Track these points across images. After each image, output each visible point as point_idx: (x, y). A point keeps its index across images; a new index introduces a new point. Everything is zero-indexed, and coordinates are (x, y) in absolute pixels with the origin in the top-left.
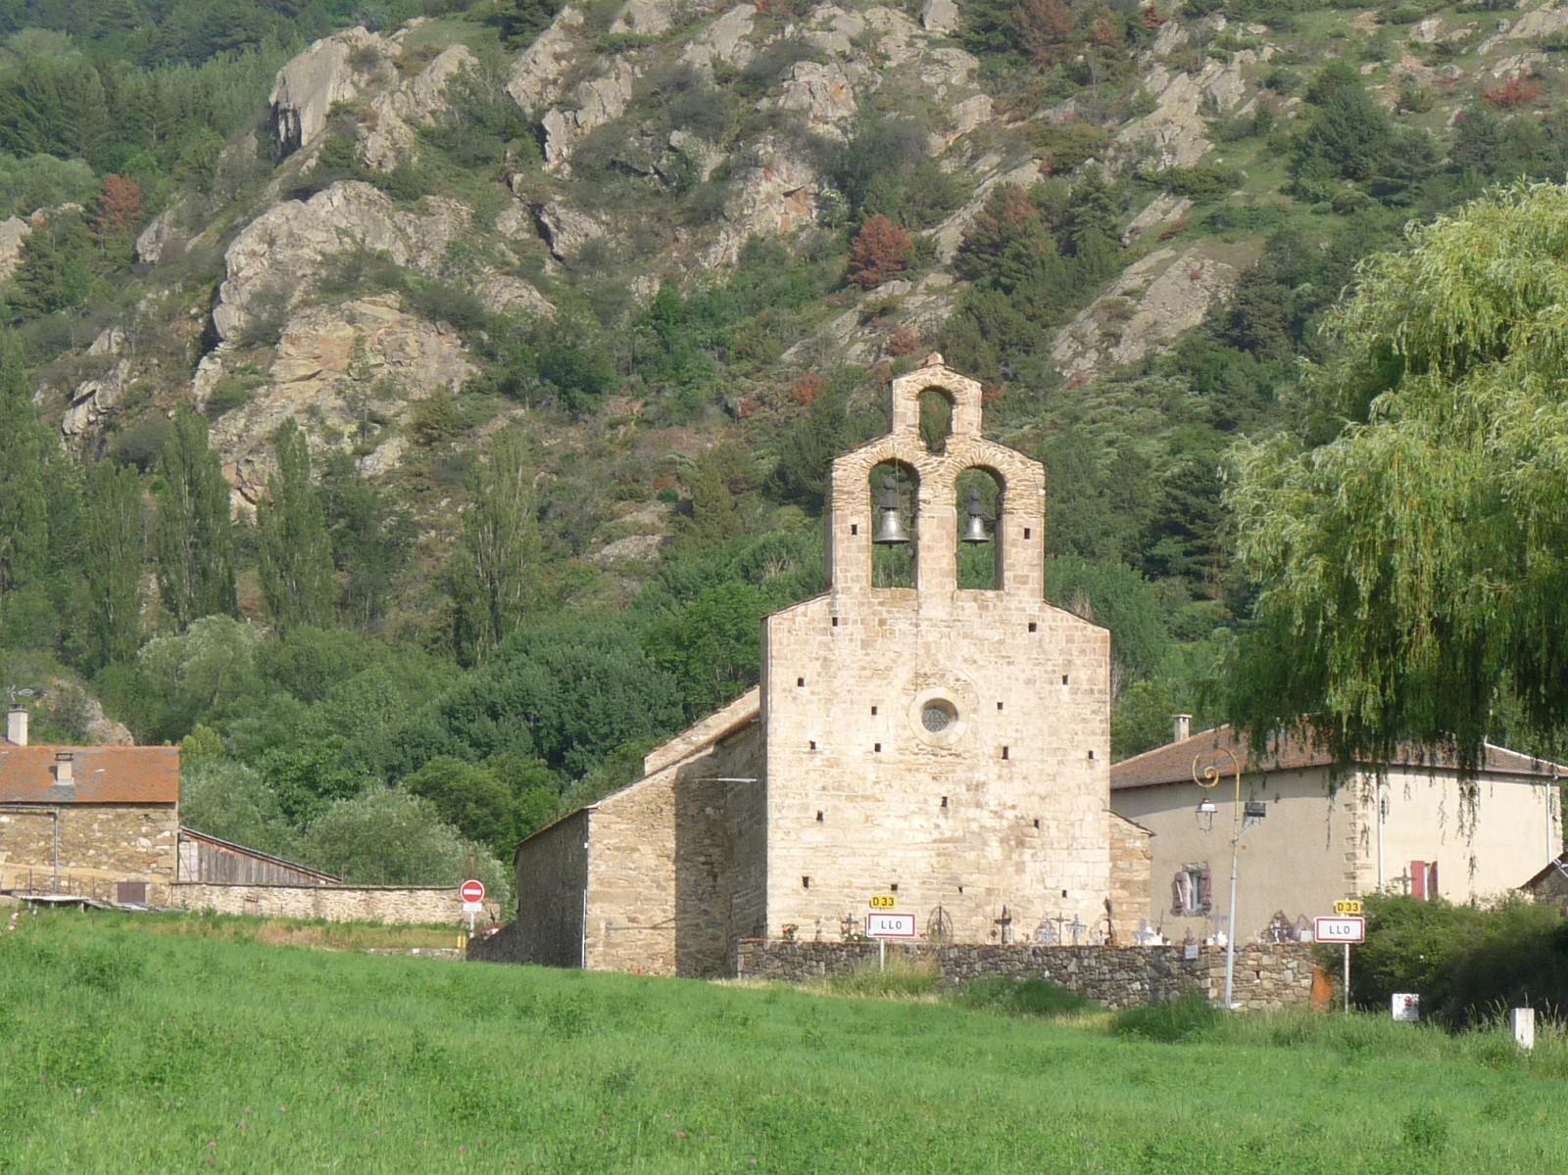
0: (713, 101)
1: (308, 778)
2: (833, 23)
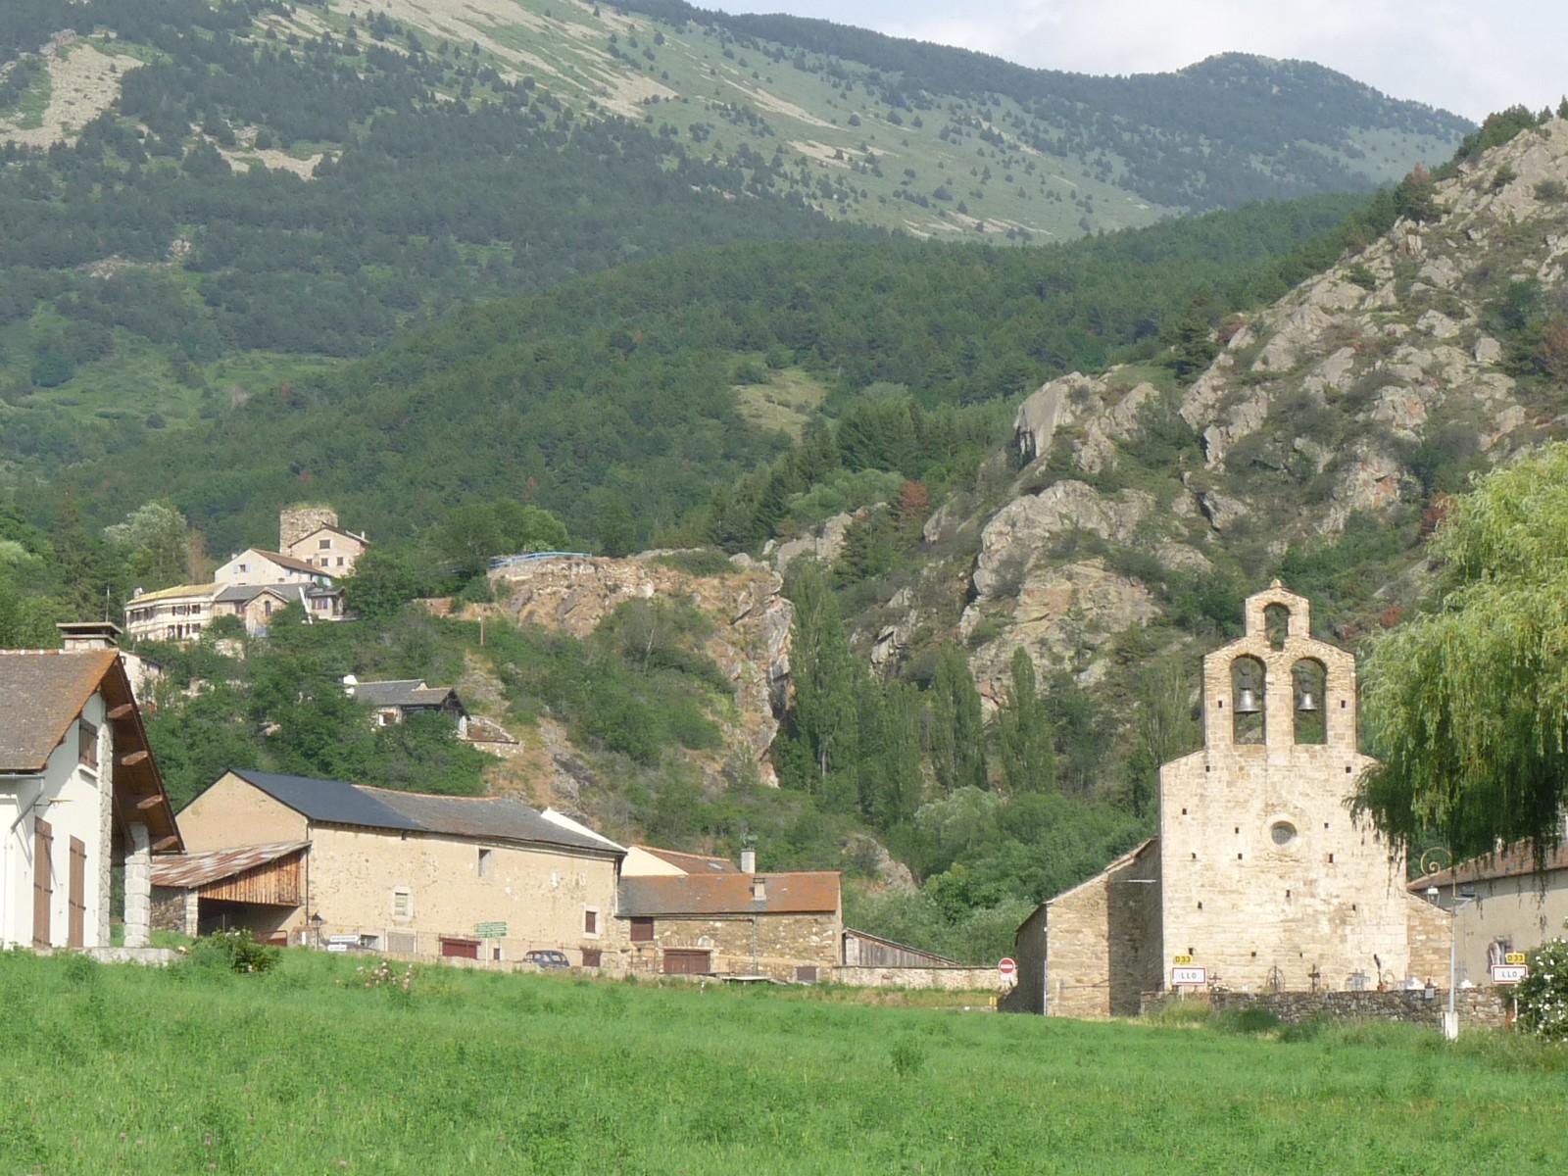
0: (1325, 416)
1: (964, 895)
2: (1410, 358)
